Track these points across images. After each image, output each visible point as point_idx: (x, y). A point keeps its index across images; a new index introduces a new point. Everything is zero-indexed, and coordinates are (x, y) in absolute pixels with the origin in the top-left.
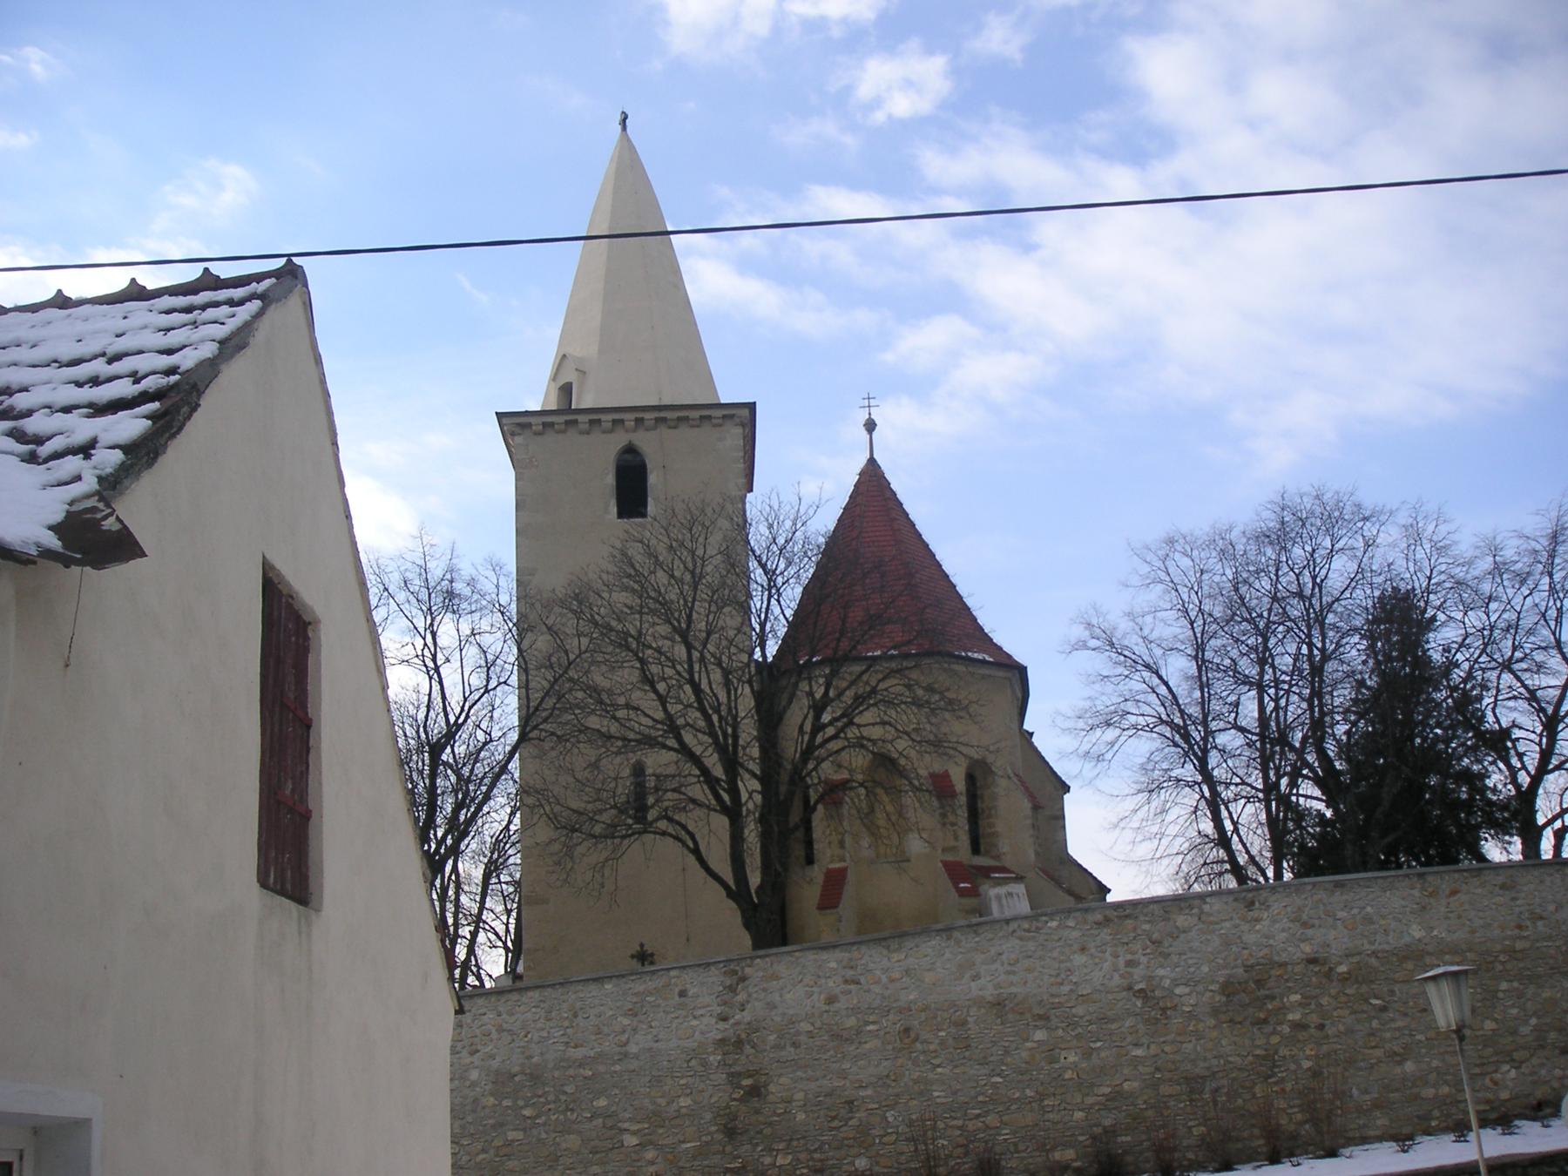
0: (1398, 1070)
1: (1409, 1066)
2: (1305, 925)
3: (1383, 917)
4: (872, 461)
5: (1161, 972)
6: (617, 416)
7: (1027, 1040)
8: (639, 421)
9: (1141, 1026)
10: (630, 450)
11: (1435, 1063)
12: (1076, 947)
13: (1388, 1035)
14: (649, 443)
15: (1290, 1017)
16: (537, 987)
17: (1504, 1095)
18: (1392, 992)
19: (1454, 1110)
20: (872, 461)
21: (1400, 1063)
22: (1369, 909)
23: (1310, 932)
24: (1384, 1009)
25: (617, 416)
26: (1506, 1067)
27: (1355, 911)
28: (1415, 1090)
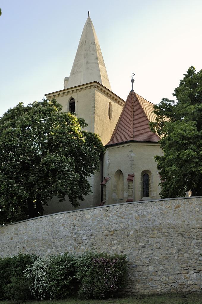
0: (147, 268)
1: (151, 268)
2: (122, 218)
3: (149, 215)
4: (132, 91)
5: (80, 232)
6: (59, 93)
7: (46, 252)
8: (73, 91)
9: (73, 249)
10: (72, 99)
11: (161, 268)
12: (61, 224)
13: (144, 256)
14: (74, 96)
15: (113, 248)
16: (159, 295)
17: (190, 283)
18: (148, 241)
19: (167, 286)
20: (132, 91)
21: (148, 266)
22: (145, 213)
23: (123, 220)
24: (143, 247)
25: (59, 93)
26: (192, 272)
27: (140, 213)
28: (152, 277)
